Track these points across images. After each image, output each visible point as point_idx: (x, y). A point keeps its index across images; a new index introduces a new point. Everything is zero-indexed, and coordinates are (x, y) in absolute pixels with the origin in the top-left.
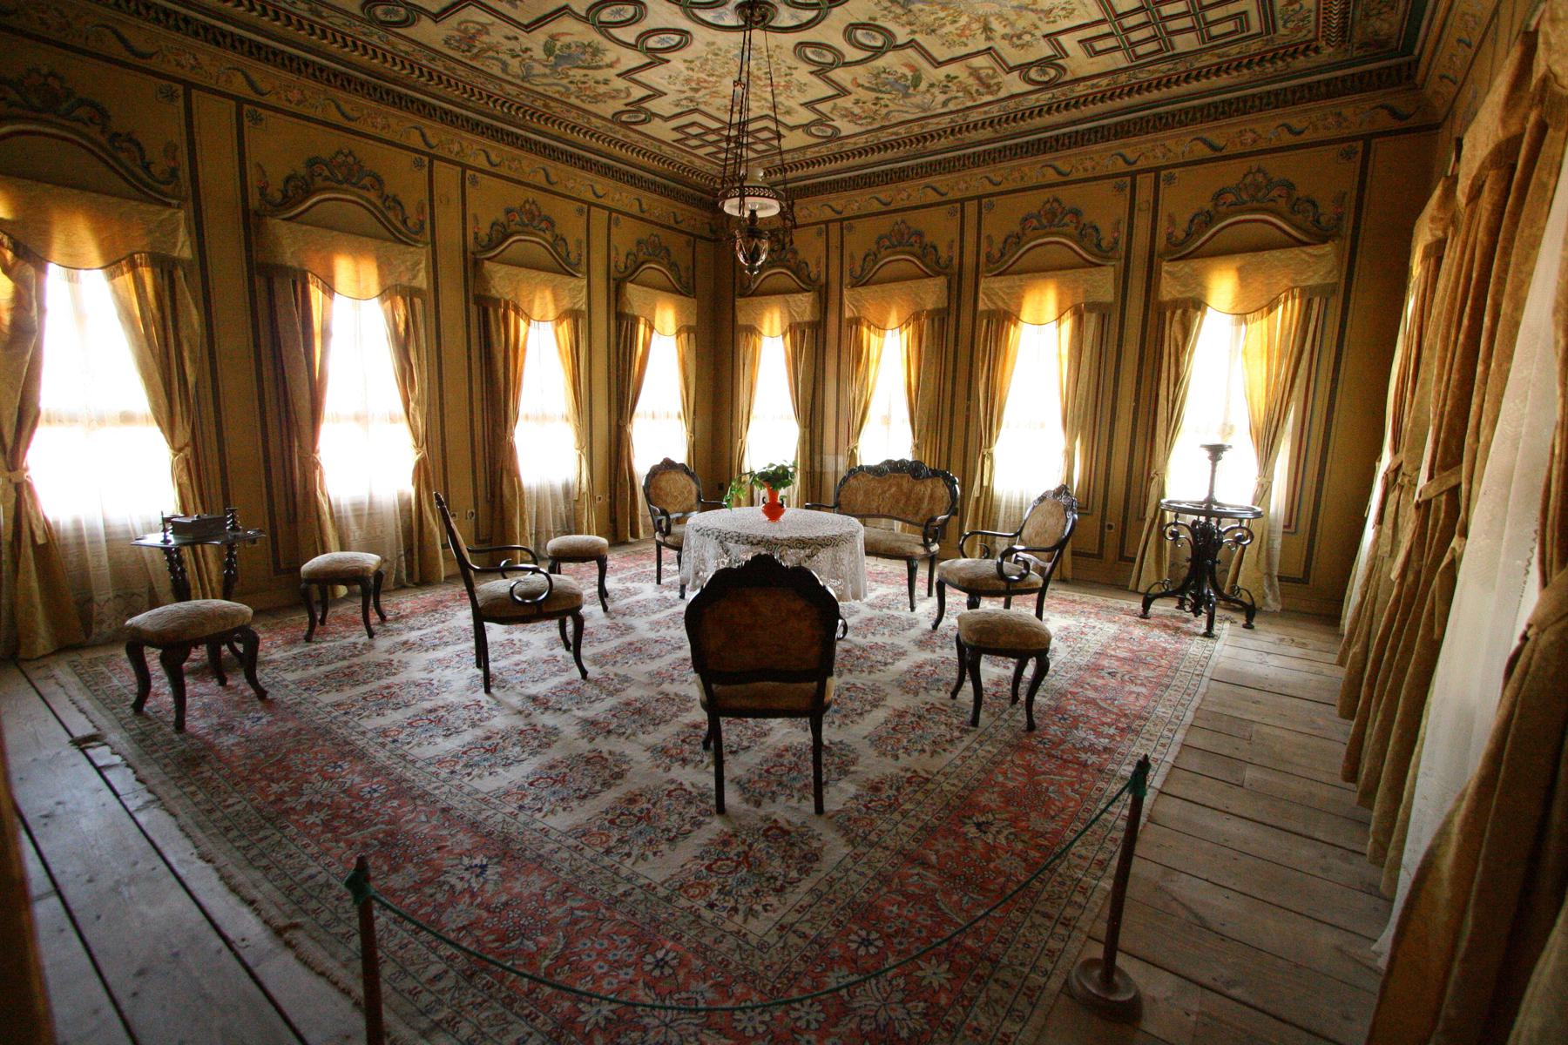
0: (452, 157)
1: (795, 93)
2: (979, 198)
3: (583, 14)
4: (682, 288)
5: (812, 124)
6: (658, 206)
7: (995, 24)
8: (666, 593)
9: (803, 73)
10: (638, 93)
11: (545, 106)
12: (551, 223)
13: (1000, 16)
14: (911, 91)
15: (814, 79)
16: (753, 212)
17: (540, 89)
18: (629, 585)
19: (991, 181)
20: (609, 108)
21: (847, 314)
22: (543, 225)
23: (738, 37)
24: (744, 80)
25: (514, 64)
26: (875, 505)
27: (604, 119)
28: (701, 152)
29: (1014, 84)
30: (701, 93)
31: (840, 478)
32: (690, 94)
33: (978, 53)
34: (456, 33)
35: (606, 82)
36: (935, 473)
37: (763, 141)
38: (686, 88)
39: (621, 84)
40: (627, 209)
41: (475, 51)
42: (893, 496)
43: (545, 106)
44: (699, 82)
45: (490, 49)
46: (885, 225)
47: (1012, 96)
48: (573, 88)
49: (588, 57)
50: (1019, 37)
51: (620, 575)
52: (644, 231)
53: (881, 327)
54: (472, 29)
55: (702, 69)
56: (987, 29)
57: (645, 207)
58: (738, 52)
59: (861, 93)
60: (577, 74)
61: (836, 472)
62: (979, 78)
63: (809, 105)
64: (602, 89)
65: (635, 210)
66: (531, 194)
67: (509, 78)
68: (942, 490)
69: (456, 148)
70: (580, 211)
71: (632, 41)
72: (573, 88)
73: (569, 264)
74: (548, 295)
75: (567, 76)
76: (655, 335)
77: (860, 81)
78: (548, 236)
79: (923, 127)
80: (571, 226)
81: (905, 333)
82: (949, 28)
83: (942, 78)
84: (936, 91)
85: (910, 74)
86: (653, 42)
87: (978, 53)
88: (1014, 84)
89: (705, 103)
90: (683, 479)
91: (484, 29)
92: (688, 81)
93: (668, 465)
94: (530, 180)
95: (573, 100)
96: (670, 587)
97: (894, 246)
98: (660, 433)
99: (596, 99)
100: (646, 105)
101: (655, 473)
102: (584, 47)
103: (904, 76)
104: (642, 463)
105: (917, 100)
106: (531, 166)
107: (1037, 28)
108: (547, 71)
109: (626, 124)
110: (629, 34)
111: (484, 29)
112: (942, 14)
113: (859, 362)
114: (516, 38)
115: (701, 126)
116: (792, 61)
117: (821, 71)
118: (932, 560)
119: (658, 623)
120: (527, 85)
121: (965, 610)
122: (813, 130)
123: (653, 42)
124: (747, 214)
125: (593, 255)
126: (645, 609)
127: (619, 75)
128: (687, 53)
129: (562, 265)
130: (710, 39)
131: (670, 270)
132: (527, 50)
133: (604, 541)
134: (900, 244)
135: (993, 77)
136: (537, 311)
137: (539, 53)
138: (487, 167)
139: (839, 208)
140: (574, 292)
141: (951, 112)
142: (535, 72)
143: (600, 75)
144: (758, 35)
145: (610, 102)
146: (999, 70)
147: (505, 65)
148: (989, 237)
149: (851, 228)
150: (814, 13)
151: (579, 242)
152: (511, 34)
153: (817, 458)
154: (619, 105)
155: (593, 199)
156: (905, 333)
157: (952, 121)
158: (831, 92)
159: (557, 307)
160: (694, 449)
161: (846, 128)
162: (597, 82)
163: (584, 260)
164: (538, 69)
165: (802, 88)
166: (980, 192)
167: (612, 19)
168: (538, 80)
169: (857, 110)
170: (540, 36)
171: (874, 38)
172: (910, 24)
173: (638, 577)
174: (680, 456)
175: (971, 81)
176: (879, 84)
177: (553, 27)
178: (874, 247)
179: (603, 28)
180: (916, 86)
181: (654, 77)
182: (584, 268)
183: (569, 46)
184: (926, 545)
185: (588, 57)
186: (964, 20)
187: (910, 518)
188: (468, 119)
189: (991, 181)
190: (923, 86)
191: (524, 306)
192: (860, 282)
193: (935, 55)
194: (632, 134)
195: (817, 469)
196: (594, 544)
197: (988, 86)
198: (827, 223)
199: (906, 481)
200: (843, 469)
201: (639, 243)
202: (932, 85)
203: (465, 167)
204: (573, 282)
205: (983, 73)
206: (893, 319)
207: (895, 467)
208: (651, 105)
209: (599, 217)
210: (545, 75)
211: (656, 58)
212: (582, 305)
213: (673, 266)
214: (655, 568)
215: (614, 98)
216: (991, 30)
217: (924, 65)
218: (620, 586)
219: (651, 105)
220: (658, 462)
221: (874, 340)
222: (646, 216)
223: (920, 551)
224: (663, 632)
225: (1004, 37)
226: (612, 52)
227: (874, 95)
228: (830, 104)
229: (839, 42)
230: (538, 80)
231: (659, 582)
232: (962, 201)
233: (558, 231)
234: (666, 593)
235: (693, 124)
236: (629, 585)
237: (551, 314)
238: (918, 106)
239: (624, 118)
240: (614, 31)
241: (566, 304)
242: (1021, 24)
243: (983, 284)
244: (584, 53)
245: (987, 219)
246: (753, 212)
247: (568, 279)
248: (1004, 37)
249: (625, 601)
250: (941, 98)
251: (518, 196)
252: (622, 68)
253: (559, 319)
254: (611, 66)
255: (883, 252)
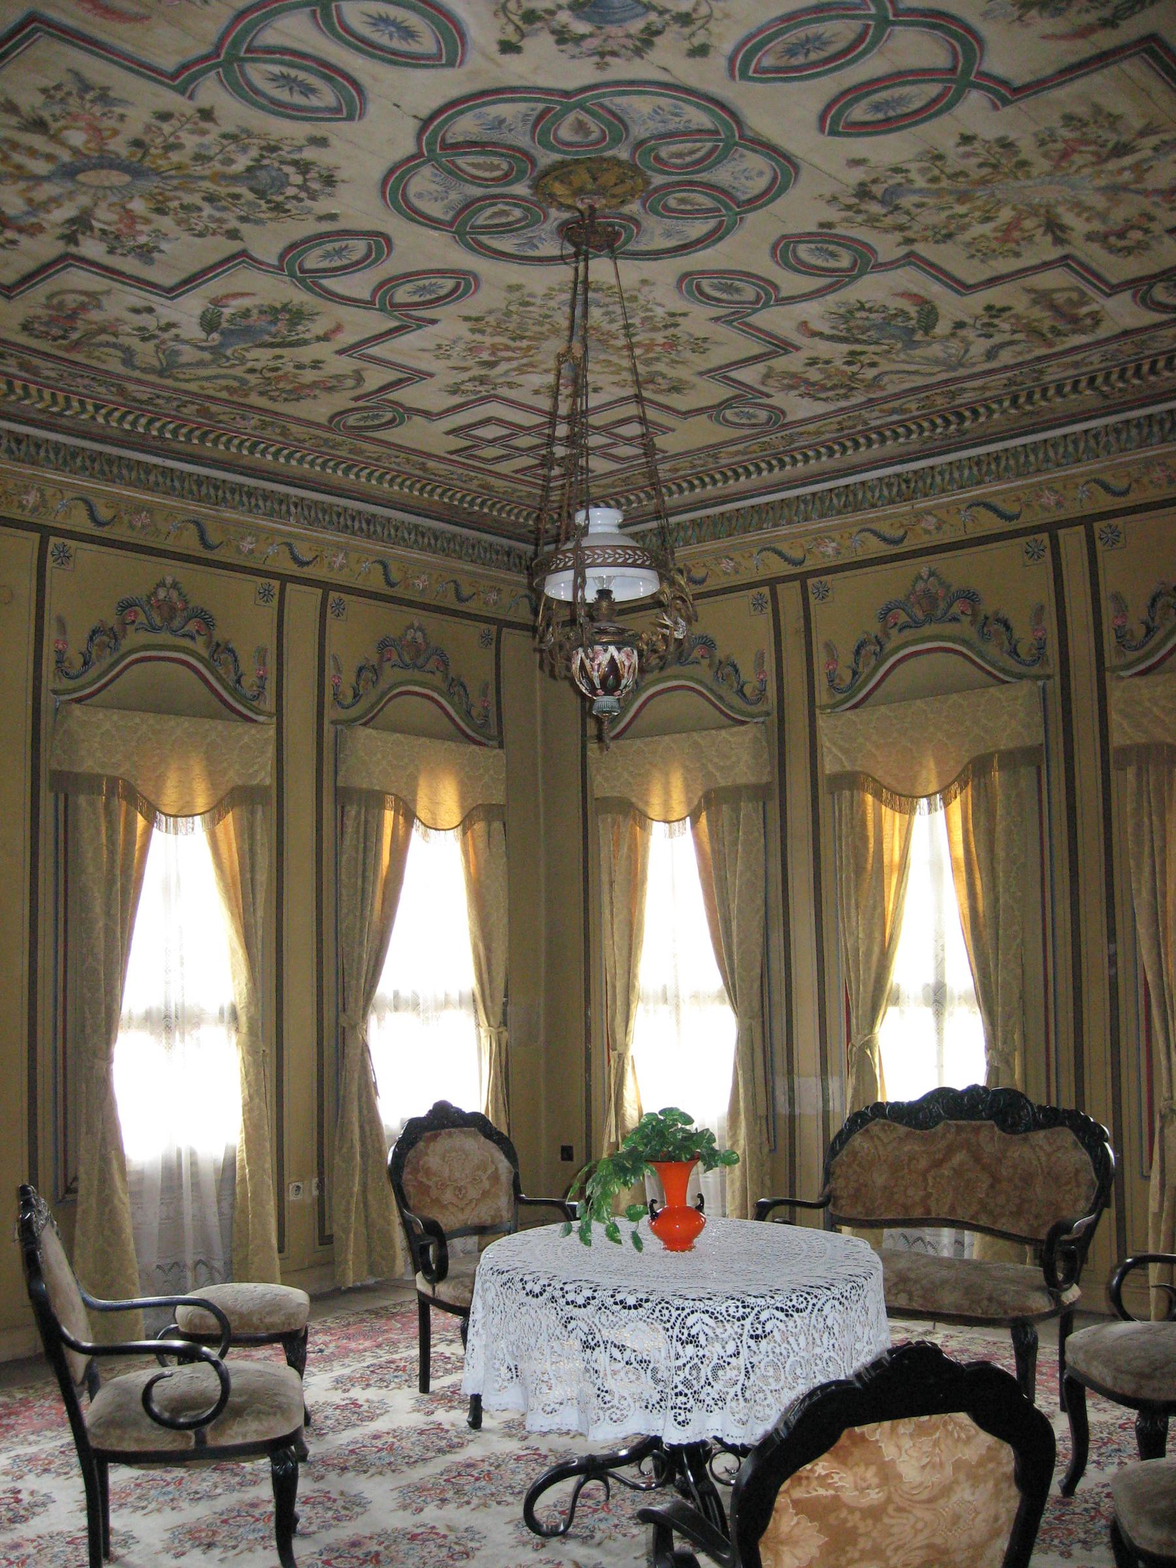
0: (27, 517)
1: (688, 354)
2: (1087, 521)
3: (276, 263)
4: (477, 725)
5: (725, 404)
6: (422, 570)
7: (1068, 218)
8: (442, 1416)
9: (698, 319)
10: (375, 378)
11: (203, 412)
12: (206, 620)
13: (1079, 207)
14: (919, 336)
15: (722, 330)
16: (604, 594)
17: (193, 387)
18: (357, 1393)
19: (1106, 488)
20: (320, 409)
21: (829, 766)
22: (192, 627)
23: (564, 273)
24: (577, 351)
25: (146, 352)
26: (916, 1194)
27: (318, 425)
28: (505, 468)
29: (1123, 312)
30: (503, 367)
31: (836, 1127)
32: (477, 372)
33: (1046, 266)
34: (40, 312)
35: (316, 365)
36: (1052, 1118)
37: (629, 441)
38: (470, 363)
39: (345, 365)
40: (359, 583)
41: (75, 336)
42: (958, 1172)
43: (203, 412)
44: (494, 349)
45: (103, 330)
46: (893, 582)
47: (1126, 333)
48: (253, 379)
49: (282, 327)
50: (1121, 235)
51: (339, 1371)
52: (393, 622)
53: (904, 800)
54: (71, 300)
55: (499, 329)
56: (1055, 229)
57: (395, 576)
58: (567, 296)
59: (824, 349)
60: (263, 357)
61: (826, 1116)
62: (1053, 307)
63: (720, 373)
64: (309, 376)
65: (376, 582)
66: (172, 571)
67: (137, 374)
68: (1069, 1153)
69: (32, 499)
70: (266, 594)
71: (366, 295)
72: (253, 379)
73: (243, 699)
74: (198, 769)
75: (243, 360)
76: (416, 834)
77: (816, 325)
78: (199, 646)
79: (953, 395)
80: (244, 616)
81: (956, 806)
82: (978, 230)
83: (980, 311)
84: (969, 334)
85: (913, 311)
86: (402, 295)
87: (1046, 266)
88: (1123, 312)
89: (510, 385)
90: (474, 1145)
91: (94, 299)
92: (473, 349)
93: (443, 1118)
94: (168, 544)
95: (255, 400)
96: (450, 1398)
97: (918, 624)
98: (429, 1047)
99: (298, 393)
100: (394, 396)
101: (416, 1130)
102: (273, 313)
103: (902, 313)
104: (398, 1105)
105: (936, 350)
106: (171, 516)
107: (1152, 219)
108: (207, 356)
109: (357, 432)
110: (359, 285)
111: (94, 299)
112: (961, 209)
113: (859, 870)
114: (150, 310)
115: (501, 422)
116: (678, 303)
117: (736, 319)
118: (1067, 1320)
119: (420, 1489)
120: (169, 382)
121: (1134, 1464)
122: (729, 414)
123: (402, 295)
124: (591, 595)
125: (289, 685)
126: (385, 1457)
127: (340, 352)
128: (473, 305)
129: (230, 693)
130: (514, 280)
131: (448, 695)
132: (170, 325)
133: (299, 1296)
134: (930, 618)
135: (1082, 303)
136: (170, 797)
137: (192, 330)
138: (89, 528)
139: (797, 554)
140: (250, 752)
141: (1006, 368)
142: (183, 359)
143: (307, 354)
144: (601, 269)
145: (324, 396)
146: (1091, 292)
147: (128, 358)
148: (1117, 598)
149: (823, 594)
150: (712, 224)
151: (262, 653)
152: (140, 303)
153: (781, 1084)
154: (341, 400)
155: (292, 569)
156: (956, 806)
157: (1011, 382)
158: (756, 349)
159: (214, 786)
160: (507, 1073)
161: (799, 407)
162: (300, 366)
163: (271, 686)
164: (189, 354)
165: (700, 345)
166: (1089, 509)
167: (325, 264)
168: (190, 373)
169: (814, 375)
170: (192, 305)
171: (833, 255)
172: (901, 228)
173: (378, 1375)
174: (473, 1094)
175: (1037, 313)
176: (851, 328)
177: (215, 287)
178: (875, 628)
179: (309, 280)
180: (928, 328)
181: (408, 348)
182: (269, 704)
183: (246, 313)
184: (1053, 1287)
185: (282, 327)
186: (1006, 215)
187: (1004, 1225)
188: (57, 447)
189: (1106, 488)
190: (942, 327)
191: (145, 788)
192: (854, 694)
193: (958, 273)
194: (365, 446)
195: (782, 1108)
196: (275, 1306)
197: (1074, 320)
198: (772, 583)
199: (989, 1137)
200: (842, 1109)
201: (384, 645)
202: (960, 325)
203: (46, 532)
204: (247, 734)
205: (1060, 298)
206: (930, 778)
207: (945, 1105)
208: (407, 396)
209: (303, 601)
210: (201, 364)
211: (408, 320)
212: (266, 778)
213: (455, 686)
214: (416, 1352)
215: (330, 389)
216: (1063, 228)
217: (934, 290)
218: (337, 1397)
219: (407, 396)
220: (421, 1110)
221: (891, 820)
222: (398, 592)
223: (1040, 1303)
224: (432, 1514)
225: (1090, 237)
226: (329, 314)
227: (845, 348)
228: (761, 368)
229: (766, 267)
230: (190, 373)
231: (424, 1388)
232: (1052, 529)
233: (218, 635)
234: (442, 1416)
235: (487, 421)
236: (357, 1393)
237: (201, 802)
238: (937, 362)
239: (351, 421)
240: (326, 282)
241: (233, 778)
242: (1119, 215)
243: (1116, 694)
244: (274, 322)
245: (1108, 561)
246: (604, 594)
247: (240, 728)
248: (1090, 237)
249: (345, 1437)
250: (980, 346)
251: (139, 576)
252: (347, 338)
253: (215, 813)
254: (325, 338)
255: (896, 638)
